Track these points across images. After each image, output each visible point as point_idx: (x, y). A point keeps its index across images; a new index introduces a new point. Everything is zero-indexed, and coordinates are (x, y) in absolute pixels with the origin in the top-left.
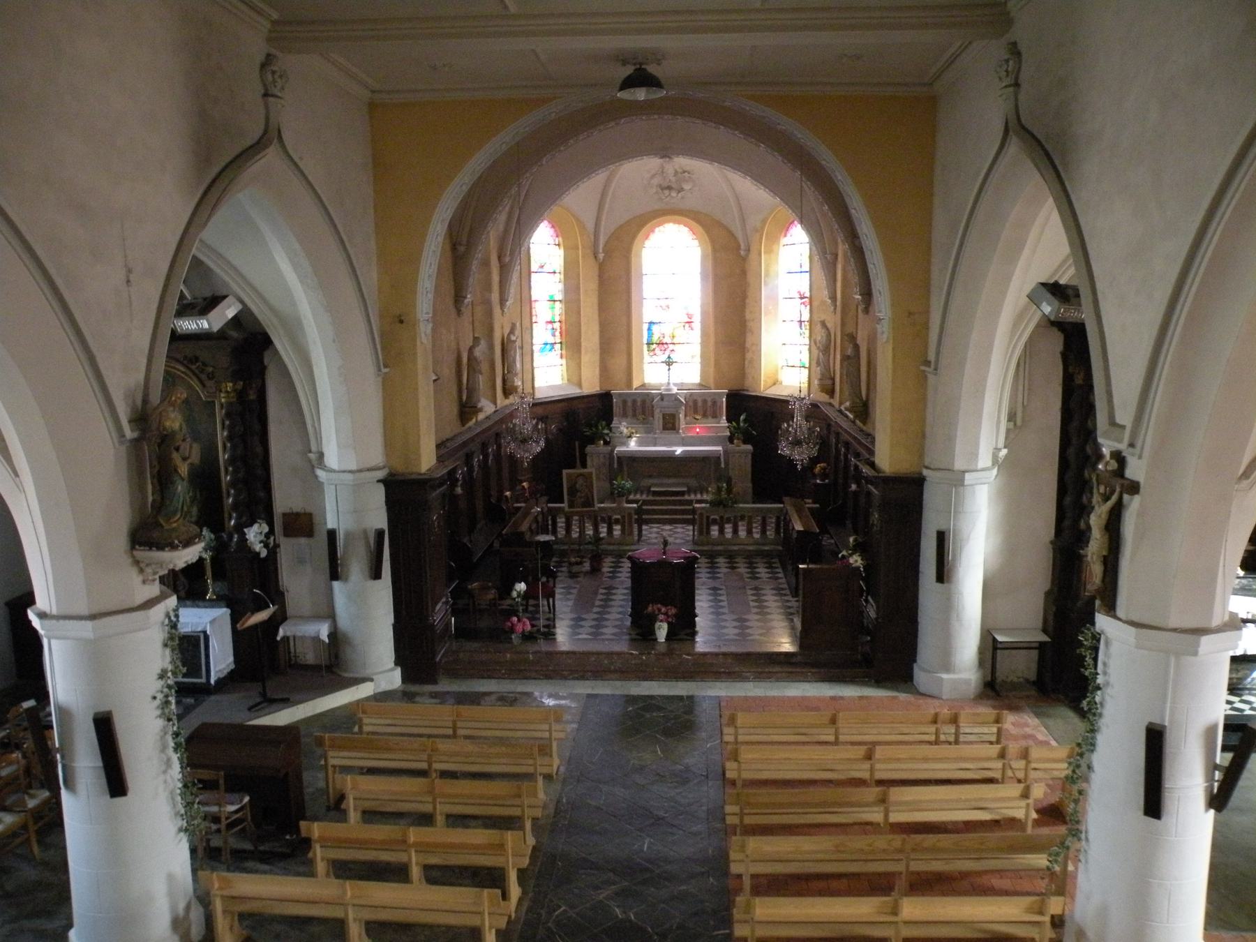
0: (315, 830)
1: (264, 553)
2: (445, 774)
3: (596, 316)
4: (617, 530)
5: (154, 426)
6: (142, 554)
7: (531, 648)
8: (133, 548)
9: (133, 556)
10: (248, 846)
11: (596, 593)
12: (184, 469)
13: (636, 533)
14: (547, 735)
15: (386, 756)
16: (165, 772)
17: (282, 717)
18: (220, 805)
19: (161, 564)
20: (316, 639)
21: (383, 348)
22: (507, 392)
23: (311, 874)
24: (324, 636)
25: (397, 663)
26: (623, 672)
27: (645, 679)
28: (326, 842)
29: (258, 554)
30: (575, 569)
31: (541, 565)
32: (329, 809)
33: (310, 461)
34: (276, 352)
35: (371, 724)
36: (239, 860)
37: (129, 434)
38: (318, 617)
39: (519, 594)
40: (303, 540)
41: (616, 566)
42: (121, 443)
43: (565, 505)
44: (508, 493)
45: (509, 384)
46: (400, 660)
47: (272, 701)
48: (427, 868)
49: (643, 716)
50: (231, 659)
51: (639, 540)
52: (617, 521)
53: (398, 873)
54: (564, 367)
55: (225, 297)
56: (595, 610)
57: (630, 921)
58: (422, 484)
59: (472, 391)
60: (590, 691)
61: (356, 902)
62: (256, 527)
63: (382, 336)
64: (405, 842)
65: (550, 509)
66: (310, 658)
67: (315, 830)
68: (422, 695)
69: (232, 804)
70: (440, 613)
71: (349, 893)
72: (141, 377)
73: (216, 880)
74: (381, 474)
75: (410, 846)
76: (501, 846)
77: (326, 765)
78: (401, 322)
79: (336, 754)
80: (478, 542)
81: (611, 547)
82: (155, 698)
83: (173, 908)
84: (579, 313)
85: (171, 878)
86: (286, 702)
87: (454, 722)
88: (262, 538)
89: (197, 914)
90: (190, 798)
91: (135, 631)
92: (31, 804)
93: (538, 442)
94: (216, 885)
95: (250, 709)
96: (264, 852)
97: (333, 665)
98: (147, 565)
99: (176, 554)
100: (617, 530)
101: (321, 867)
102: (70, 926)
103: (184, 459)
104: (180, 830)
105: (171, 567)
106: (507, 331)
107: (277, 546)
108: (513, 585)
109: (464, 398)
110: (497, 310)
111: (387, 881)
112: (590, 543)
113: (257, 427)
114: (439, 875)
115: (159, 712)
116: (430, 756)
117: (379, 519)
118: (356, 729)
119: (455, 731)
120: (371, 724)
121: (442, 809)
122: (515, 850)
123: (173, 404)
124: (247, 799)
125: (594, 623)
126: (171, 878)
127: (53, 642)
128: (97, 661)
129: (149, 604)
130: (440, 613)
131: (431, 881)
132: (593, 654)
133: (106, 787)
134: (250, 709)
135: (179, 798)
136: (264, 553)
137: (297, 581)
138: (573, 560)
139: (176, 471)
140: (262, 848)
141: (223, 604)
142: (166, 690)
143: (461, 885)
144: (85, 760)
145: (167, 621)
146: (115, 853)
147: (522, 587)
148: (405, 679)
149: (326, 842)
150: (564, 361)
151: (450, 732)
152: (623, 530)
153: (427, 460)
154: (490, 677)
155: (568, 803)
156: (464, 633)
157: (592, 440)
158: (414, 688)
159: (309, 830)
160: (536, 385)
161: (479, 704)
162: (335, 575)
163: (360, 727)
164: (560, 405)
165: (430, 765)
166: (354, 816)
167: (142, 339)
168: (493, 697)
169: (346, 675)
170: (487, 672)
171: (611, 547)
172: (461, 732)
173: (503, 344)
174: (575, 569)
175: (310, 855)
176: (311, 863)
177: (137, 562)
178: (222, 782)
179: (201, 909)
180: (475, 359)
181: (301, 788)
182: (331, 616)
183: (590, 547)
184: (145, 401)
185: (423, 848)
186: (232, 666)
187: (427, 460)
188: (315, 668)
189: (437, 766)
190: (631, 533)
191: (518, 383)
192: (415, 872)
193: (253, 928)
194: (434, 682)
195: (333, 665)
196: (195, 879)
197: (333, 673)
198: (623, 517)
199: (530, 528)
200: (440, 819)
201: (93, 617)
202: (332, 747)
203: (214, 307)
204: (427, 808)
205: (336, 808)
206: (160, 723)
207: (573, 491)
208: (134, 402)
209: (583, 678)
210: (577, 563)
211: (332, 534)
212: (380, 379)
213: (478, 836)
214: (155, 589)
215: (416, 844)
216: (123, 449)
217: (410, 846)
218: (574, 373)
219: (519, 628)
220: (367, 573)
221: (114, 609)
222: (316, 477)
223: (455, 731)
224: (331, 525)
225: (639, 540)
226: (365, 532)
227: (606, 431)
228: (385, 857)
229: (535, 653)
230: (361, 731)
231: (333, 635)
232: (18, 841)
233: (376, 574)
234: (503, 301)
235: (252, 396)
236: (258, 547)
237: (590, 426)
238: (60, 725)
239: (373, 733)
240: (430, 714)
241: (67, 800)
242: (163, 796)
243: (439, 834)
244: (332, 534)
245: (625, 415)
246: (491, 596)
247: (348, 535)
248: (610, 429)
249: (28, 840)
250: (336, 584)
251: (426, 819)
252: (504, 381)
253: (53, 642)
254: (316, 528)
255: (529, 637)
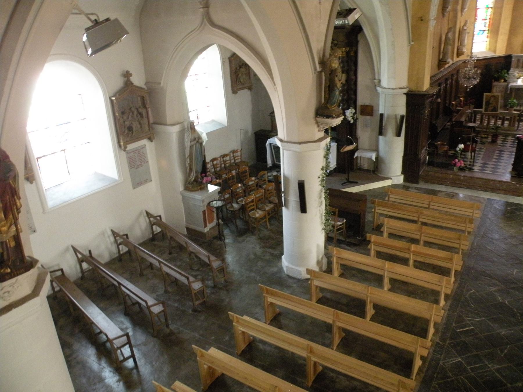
0: (373, 238)
1: (352, 121)
2: (425, 224)
3: (510, 16)
4: (506, 123)
5: (328, 67)
6: (320, 119)
7: (462, 174)
8: (316, 117)
9: (316, 120)
10: (343, 239)
11: (494, 152)
12: (339, 85)
13: (517, 126)
14: (471, 214)
15: (394, 211)
16: (320, 206)
17: (354, 189)
18: (335, 221)
19: (327, 124)
20: (370, 159)
21: (412, 33)
22: (458, 55)
23: (369, 255)
24: (374, 159)
25: (402, 173)
26: (505, 190)
27: (517, 196)
28: (376, 244)
29: (350, 121)
30: (484, 140)
31: (472, 138)
32: (373, 229)
33: (374, 83)
34: (364, 33)
35: (393, 198)
36: (339, 243)
37: (319, 69)
38: (371, 150)
39: (460, 150)
40: (368, 117)
41: (504, 141)
42: (315, 73)
43: (483, 110)
44: (454, 102)
45: (460, 51)
46: (404, 172)
47: (351, 182)
48: (415, 261)
49: (515, 213)
50: (335, 163)
51: (517, 129)
52: (507, 119)
53: (404, 261)
54: (488, 43)
55: (355, 9)
56: (494, 160)
57: (506, 304)
58: (423, 96)
59: (445, 54)
60: (489, 197)
61: (390, 270)
62: (350, 110)
63: (412, 26)
64: (409, 249)
65: (475, 112)
66: (366, 166)
67: (373, 238)
68: (412, 188)
69: (340, 222)
70: (424, 155)
71: (387, 266)
72: (322, 44)
73: (335, 251)
74: (405, 91)
75: (411, 252)
76: (451, 260)
77: (374, 212)
78: (422, 20)
79: (379, 208)
80: (439, 124)
81: (503, 132)
82: (319, 177)
83: (318, 256)
84: (501, 14)
85: (318, 246)
86: (356, 183)
87: (430, 202)
88: (352, 115)
89: (325, 261)
90: (328, 218)
91: (314, 150)
92: (267, 209)
93: (475, 79)
94: (335, 252)
95: (342, 184)
96: (348, 242)
97: (376, 171)
98: (322, 124)
99: (333, 120)
100: (506, 123)
101: (373, 253)
102: (283, 254)
103: (340, 81)
104: (323, 229)
105: (331, 125)
106: (462, 24)
107: (357, 119)
108: (458, 145)
109: (441, 57)
110: (459, 14)
111: (396, 263)
112: (493, 129)
113: (353, 68)
114: (420, 265)
115: (320, 183)
116: (419, 215)
117: (402, 110)
118: (387, 199)
119: (429, 206)
120: (393, 198)
121: (423, 238)
122: (456, 263)
123: (336, 57)
124: (345, 221)
125: (482, 165)
126: (318, 246)
127: (284, 151)
128: (300, 161)
129: (320, 140)
130: (424, 155)
131: (416, 267)
132: (492, 180)
133: (300, 209)
134: (342, 184)
135: (324, 217)
136: (352, 121)
137: (364, 135)
138: (484, 136)
139: (336, 86)
140: (348, 240)
141: (334, 141)
142: (324, 175)
143: (428, 271)
144: (293, 198)
145: (326, 148)
146: (300, 233)
147: (462, 146)
148: (405, 180)
149: (376, 244)
150: (488, 40)
151: (427, 206)
152: (510, 124)
153: (426, 86)
154: (442, 184)
155: (477, 245)
156: (431, 163)
157: (498, 79)
158: (408, 184)
159: (370, 237)
160: (473, 51)
161: (437, 195)
162: (381, 133)
163: (389, 198)
164: (484, 61)
165: (418, 219)
166: (385, 235)
167: (323, 28)
168: (443, 193)
169: (380, 175)
170: (442, 182)
171: (503, 132)
172: (431, 207)
173: (459, 31)
174: (484, 140)
175: (369, 247)
176: (369, 250)
177: (317, 123)
178: (337, 213)
179: (326, 259)
180: (449, 38)
181: (365, 218)
182: (377, 150)
183: (493, 131)
184: (324, 55)
185: (416, 253)
186: (336, 166)
187: (426, 86)
188: (368, 171)
189: (421, 220)
190: (514, 126)
191: (465, 50)
192: (411, 262)
193: (344, 270)
194: (417, 182)
195: (376, 171)
196: (326, 248)
197: (376, 174)
198: (511, 118)
199: (466, 120)
200: (422, 243)
201: (300, 143)
202: (378, 205)
203: (351, 13)
204: (418, 237)
205: (378, 229)
206: (320, 187)
207: (488, 103)
208: (320, 55)
209: (486, 191)
210: (485, 138)
211: (382, 115)
212: (409, 47)
213: (400, 244)
214: (322, 134)
215: (414, 252)
216: (315, 75)
217: (411, 252)
218: (493, 47)
219: (458, 164)
220: (395, 134)
221: (307, 141)
222: (376, 90)
223: (429, 206)
224: (381, 111)
225: (517, 129)
226: (396, 116)
227: (506, 75)
228: (399, 254)
229: (464, 176)
230: (388, 200)
231: (377, 158)
232: (263, 221)
233: (399, 135)
234: (462, 9)
235: (352, 54)
236: (350, 119)
237: (497, 72)
238: (284, 183)
239: (393, 201)
240: (416, 197)
241: (285, 211)
242: (318, 215)
243: (421, 248)
244: (382, 115)
245: (517, 67)
246: (446, 149)
247: (388, 116)
248: (508, 74)
249: (266, 222)
250: (380, 137)
251: (415, 241)
252: (458, 49)
253: (284, 151)
254: (374, 113)
255: (461, 169)
